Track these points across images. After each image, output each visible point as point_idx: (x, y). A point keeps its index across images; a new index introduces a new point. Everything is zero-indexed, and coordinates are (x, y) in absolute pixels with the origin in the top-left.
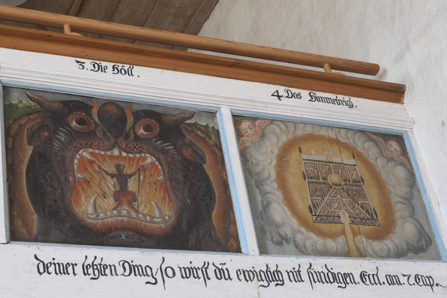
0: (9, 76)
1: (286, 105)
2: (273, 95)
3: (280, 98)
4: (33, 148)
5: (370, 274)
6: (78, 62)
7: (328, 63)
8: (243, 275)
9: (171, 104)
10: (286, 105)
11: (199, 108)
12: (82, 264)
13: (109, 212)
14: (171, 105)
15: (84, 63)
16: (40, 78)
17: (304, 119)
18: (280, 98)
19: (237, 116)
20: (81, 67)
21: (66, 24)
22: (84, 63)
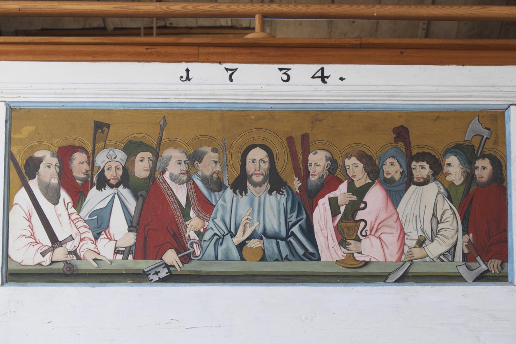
0: (282, 98)
1: (39, 90)
2: (313, 77)
3: (326, 79)
4: (365, 168)
5: (243, 198)
6: (281, 69)
7: (259, 14)
8: (366, 228)
9: (407, 108)
10: (39, 90)
11: (412, 107)
12: (382, 232)
13: (101, 159)
14: (397, 109)
15: (289, 69)
16: (480, 97)
17: (475, 105)
18: (326, 79)
19: (57, 103)
20: (285, 77)
21: (256, 15)
22: (289, 69)
